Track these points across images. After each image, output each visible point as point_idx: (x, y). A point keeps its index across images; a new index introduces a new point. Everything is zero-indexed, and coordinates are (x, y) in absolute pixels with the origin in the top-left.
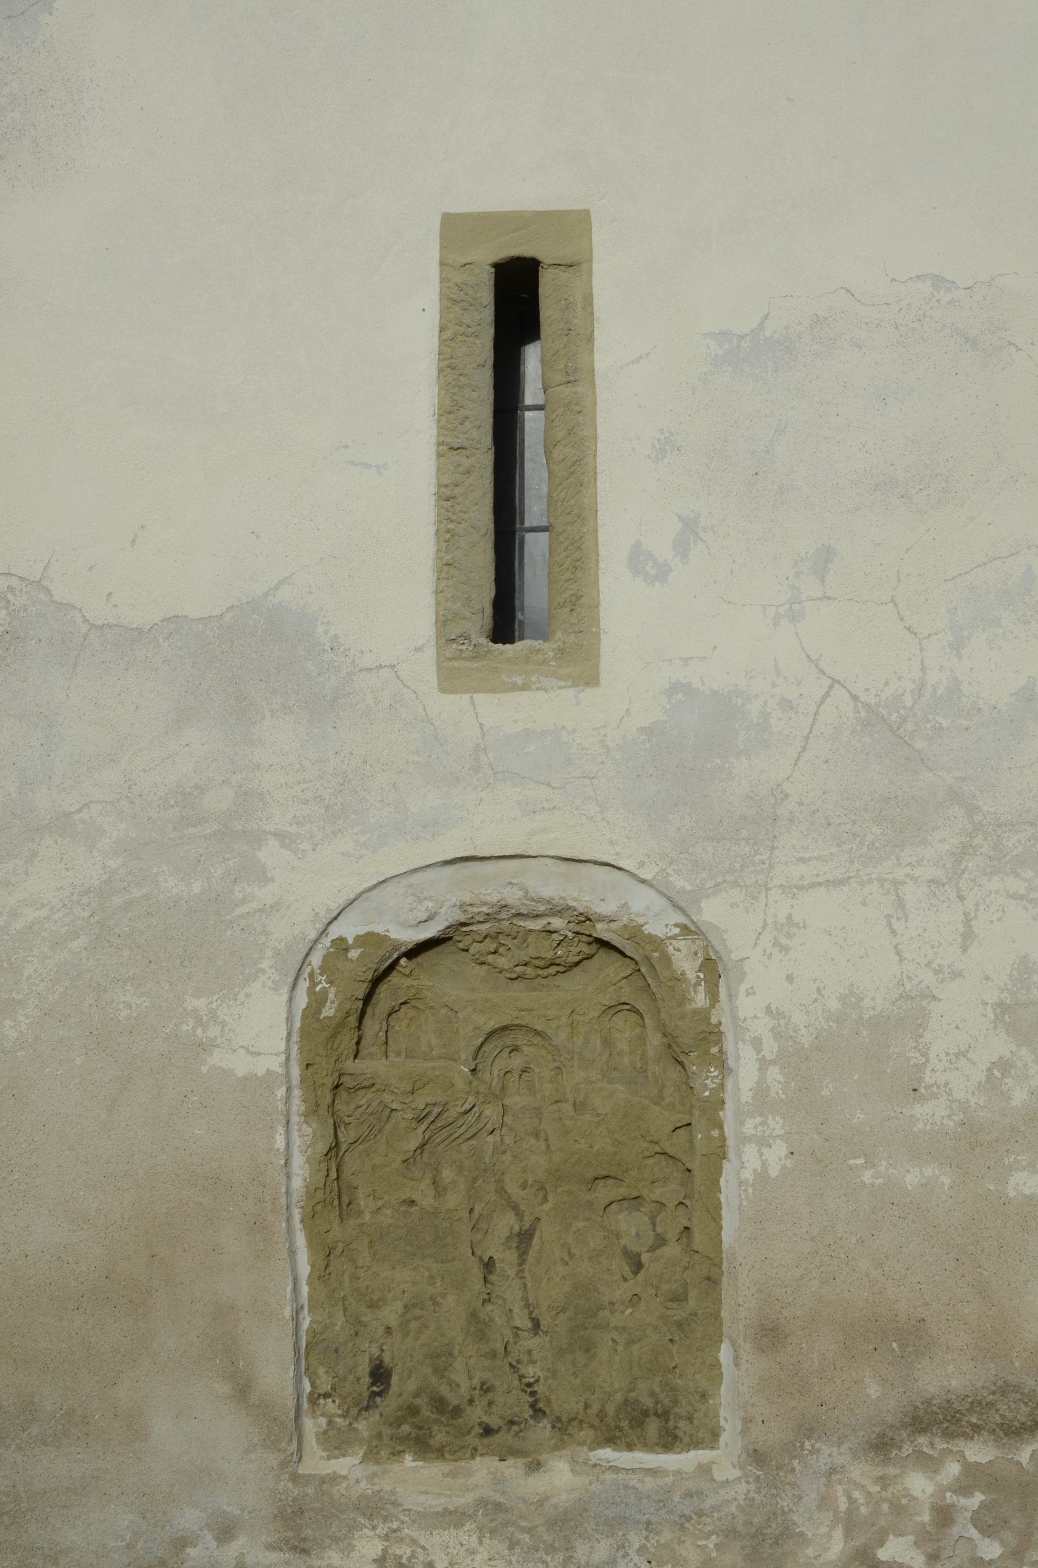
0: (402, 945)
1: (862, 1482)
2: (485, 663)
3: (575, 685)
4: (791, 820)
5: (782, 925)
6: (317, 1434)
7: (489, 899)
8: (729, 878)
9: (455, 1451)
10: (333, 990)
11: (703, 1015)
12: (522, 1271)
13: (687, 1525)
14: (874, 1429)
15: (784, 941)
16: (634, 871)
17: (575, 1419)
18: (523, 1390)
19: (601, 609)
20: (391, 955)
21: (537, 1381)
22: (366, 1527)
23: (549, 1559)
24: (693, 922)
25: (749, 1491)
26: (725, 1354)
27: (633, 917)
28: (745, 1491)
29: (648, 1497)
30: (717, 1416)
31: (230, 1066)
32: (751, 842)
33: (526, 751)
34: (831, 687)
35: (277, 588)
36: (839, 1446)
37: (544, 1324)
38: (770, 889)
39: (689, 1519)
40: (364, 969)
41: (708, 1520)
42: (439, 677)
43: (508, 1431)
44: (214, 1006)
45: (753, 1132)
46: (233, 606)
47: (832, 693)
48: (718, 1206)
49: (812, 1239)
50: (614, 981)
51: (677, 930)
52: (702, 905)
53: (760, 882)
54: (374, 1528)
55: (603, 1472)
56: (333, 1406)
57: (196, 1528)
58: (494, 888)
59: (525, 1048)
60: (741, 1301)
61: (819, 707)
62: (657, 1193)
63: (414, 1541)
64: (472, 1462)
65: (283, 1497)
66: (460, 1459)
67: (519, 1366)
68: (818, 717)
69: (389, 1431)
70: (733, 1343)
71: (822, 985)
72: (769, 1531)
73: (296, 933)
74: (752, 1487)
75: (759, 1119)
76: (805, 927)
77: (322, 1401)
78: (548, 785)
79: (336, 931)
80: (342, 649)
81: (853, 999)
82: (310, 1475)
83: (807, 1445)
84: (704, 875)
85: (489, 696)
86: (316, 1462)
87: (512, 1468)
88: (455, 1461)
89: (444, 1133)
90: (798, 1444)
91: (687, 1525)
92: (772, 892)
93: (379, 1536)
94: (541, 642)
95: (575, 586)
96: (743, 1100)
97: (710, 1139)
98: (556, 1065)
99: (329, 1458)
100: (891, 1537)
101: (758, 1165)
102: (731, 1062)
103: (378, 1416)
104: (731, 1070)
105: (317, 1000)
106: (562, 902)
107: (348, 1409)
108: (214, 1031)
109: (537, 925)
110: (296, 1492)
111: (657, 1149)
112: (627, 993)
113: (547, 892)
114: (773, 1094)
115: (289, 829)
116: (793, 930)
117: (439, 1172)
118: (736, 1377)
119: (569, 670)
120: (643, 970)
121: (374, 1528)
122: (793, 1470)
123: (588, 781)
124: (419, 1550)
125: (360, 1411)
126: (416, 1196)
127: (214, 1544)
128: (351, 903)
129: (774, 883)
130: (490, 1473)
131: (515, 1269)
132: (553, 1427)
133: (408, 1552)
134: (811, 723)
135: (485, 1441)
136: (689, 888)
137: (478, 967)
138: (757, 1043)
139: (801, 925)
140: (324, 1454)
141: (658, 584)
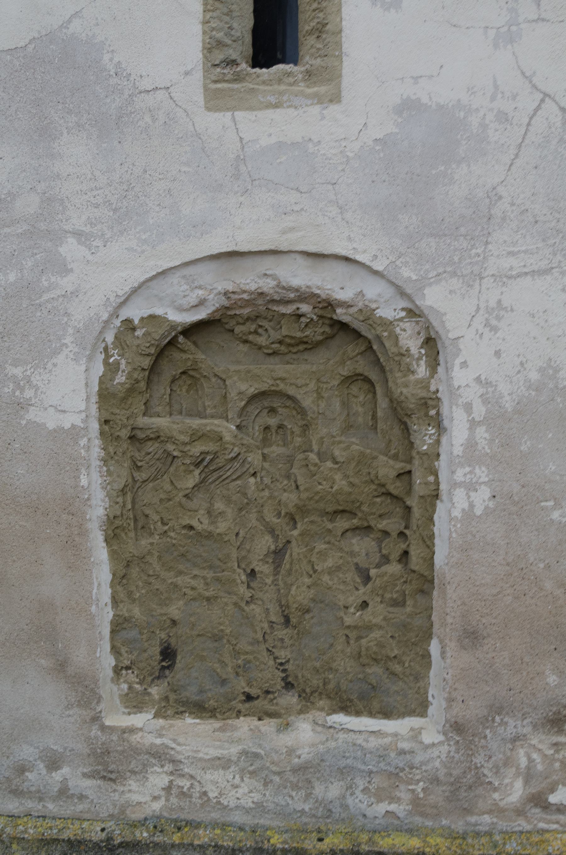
0: (178, 325)
1: (540, 746)
2: (244, 84)
3: (320, 102)
4: (504, 219)
5: (493, 309)
6: (120, 695)
7: (247, 288)
8: (449, 269)
9: (224, 713)
10: (123, 362)
11: (425, 384)
12: (277, 580)
13: (401, 774)
14: (551, 708)
15: (494, 322)
16: (368, 263)
17: (316, 691)
18: (277, 668)
19: (343, 34)
20: (170, 333)
21: (288, 661)
22: (156, 765)
23: (294, 794)
24: (417, 306)
25: (449, 752)
26: (434, 648)
27: (367, 303)
28: (446, 751)
29: (371, 753)
30: (426, 693)
31: (43, 421)
32: (468, 238)
33: (278, 161)
34: (542, 101)
35: (70, 21)
36: (523, 721)
37: (294, 621)
38: (483, 278)
39: (403, 770)
40: (148, 345)
41: (418, 771)
42: (205, 98)
43: (265, 698)
44: (28, 373)
45: (463, 480)
46: (34, 38)
47: (543, 106)
48: (432, 537)
49: (508, 564)
50: (351, 356)
51: (403, 314)
52: (425, 292)
53: (475, 272)
54: (162, 766)
55: (337, 733)
56: (132, 675)
57: (31, 759)
58: (249, 280)
59: (280, 409)
60: (448, 610)
61: (531, 118)
62: (383, 524)
63: (192, 777)
64: (237, 720)
65: (94, 742)
66: (227, 719)
67: (274, 650)
68: (530, 128)
69: (175, 697)
70: (441, 641)
71: (524, 360)
72: (465, 780)
73: (92, 315)
74: (453, 748)
75: (468, 469)
76: (512, 310)
77: (124, 672)
78: (297, 189)
79: (125, 313)
80: (125, 74)
81: (551, 372)
82: (114, 727)
83: (498, 719)
84: (427, 266)
85: (251, 115)
86: (118, 719)
87: (268, 726)
88: (224, 719)
89: (215, 475)
90: (490, 719)
91: (401, 774)
92: (485, 280)
93: (166, 773)
94: (291, 65)
95: (321, 15)
96: (455, 452)
97: (427, 484)
98: (304, 423)
99: (129, 714)
100: (560, 786)
101: (466, 506)
102: (446, 423)
103: (166, 684)
104: (445, 430)
105: (111, 369)
106: (308, 290)
107: (144, 678)
108: (29, 393)
109: (288, 310)
110: (104, 739)
111: (383, 490)
112: (362, 366)
113: (296, 282)
114: (480, 447)
115: (84, 229)
116: (502, 313)
117: (212, 505)
118: (444, 661)
119: (316, 89)
120: (375, 347)
121: (162, 766)
122: (485, 737)
123: (330, 187)
124: (196, 783)
125: (153, 680)
126: (195, 523)
127: (44, 772)
128: (136, 291)
129: (486, 274)
130: (251, 730)
131: (271, 578)
132: (300, 696)
133: (188, 784)
134: (523, 133)
135: (247, 705)
136: (414, 277)
137: (241, 345)
138: (468, 407)
139: (509, 309)
140: (126, 711)
141: (393, 11)
